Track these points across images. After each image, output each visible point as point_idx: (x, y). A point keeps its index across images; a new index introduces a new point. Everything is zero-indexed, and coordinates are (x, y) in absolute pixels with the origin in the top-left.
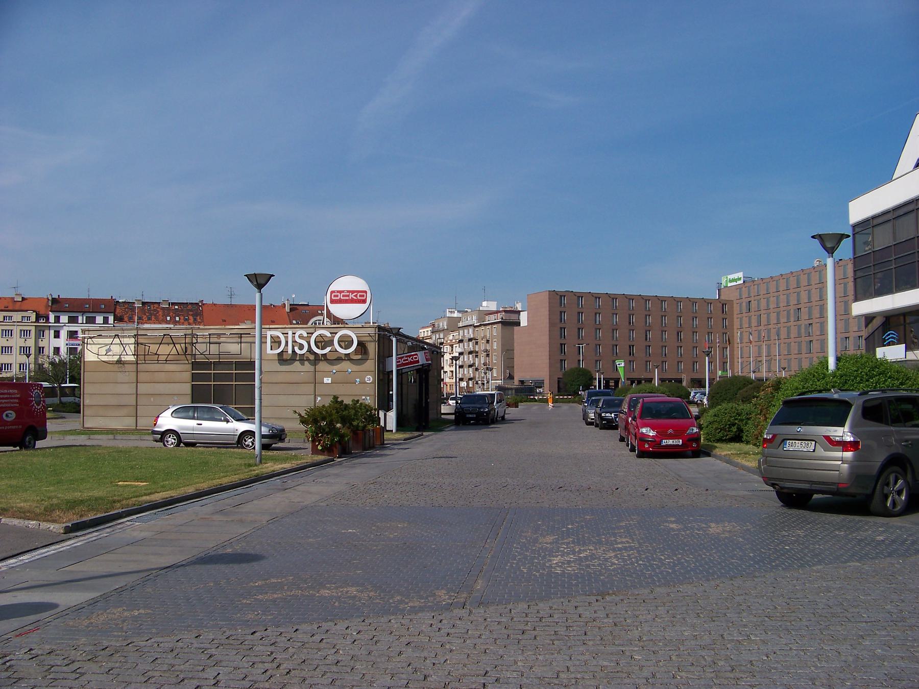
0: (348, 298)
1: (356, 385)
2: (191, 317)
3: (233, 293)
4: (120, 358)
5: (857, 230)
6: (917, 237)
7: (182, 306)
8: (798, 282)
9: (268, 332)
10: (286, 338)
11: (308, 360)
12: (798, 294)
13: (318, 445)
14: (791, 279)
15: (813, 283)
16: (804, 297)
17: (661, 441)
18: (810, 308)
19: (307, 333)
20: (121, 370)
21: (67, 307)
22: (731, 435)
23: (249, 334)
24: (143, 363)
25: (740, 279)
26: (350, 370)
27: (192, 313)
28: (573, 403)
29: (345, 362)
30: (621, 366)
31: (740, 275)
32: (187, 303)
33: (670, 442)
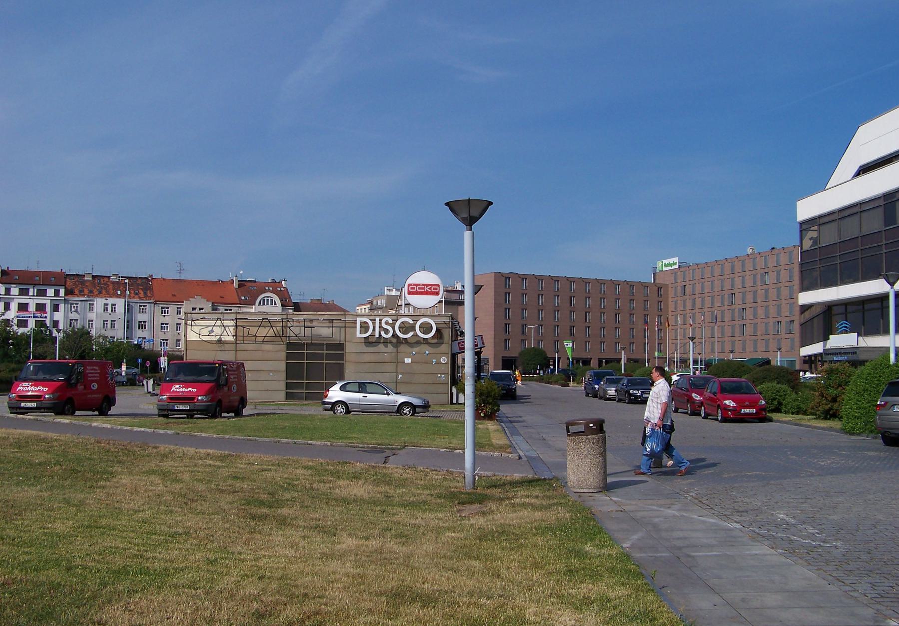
0: (423, 290)
1: (433, 365)
2: (142, 292)
3: (182, 268)
4: (220, 338)
5: (804, 227)
6: (861, 237)
7: (132, 281)
8: (733, 267)
9: (357, 318)
10: (374, 324)
11: (391, 343)
12: (733, 279)
13: (481, 413)
14: (726, 265)
15: (747, 270)
16: (738, 283)
17: (741, 410)
18: (744, 294)
19: (392, 320)
20: (221, 348)
21: (17, 279)
22: (773, 407)
23: (340, 320)
24: (241, 343)
25: (675, 264)
26: (427, 352)
27: (142, 287)
28: (530, 381)
29: (422, 345)
30: (569, 346)
31: (676, 260)
32: (137, 277)
33: (747, 411)
